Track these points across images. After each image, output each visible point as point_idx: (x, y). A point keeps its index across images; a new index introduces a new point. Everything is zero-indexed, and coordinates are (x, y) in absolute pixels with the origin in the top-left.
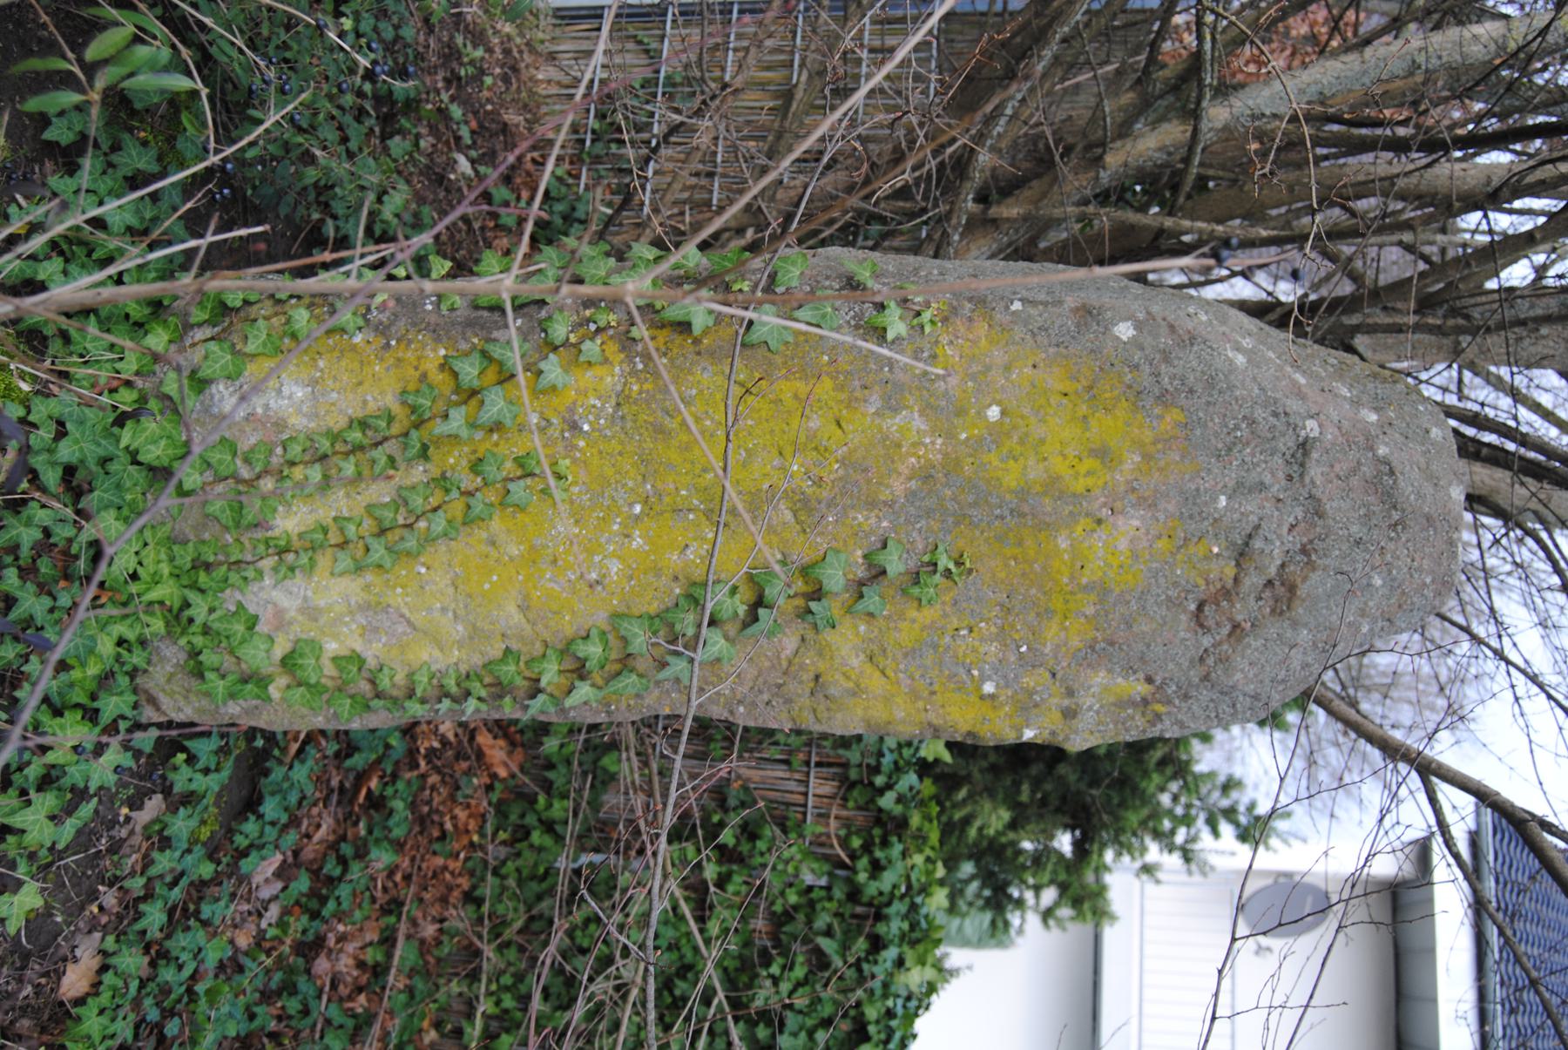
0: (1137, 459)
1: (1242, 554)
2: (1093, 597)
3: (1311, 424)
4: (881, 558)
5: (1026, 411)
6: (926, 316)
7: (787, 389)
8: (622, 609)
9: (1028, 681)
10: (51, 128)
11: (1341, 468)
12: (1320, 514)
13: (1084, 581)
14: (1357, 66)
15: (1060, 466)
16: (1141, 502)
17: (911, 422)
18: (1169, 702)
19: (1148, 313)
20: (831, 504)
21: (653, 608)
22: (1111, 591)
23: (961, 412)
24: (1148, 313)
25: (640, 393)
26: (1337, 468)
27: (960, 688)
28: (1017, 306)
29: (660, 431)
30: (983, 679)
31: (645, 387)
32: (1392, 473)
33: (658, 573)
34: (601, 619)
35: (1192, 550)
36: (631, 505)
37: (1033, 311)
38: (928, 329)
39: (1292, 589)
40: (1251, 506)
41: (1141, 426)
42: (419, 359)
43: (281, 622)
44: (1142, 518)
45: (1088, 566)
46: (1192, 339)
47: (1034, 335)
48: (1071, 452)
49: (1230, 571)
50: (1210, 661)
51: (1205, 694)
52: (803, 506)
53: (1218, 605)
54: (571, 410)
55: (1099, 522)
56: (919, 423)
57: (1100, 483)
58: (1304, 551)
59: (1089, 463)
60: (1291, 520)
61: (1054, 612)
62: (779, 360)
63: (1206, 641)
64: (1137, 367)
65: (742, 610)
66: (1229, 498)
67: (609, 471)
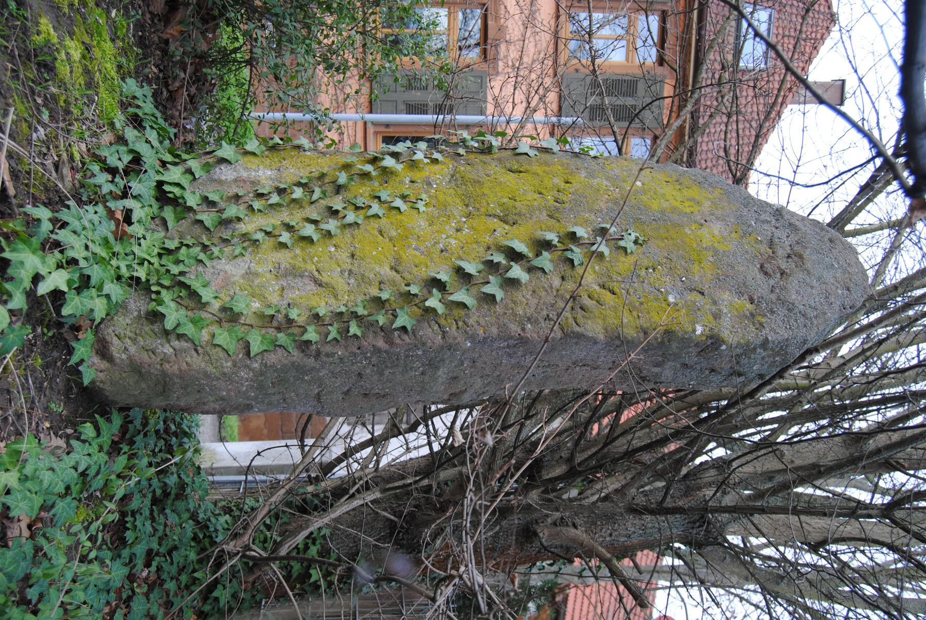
18: (764, 316)
30: (668, 293)
55: (702, 225)
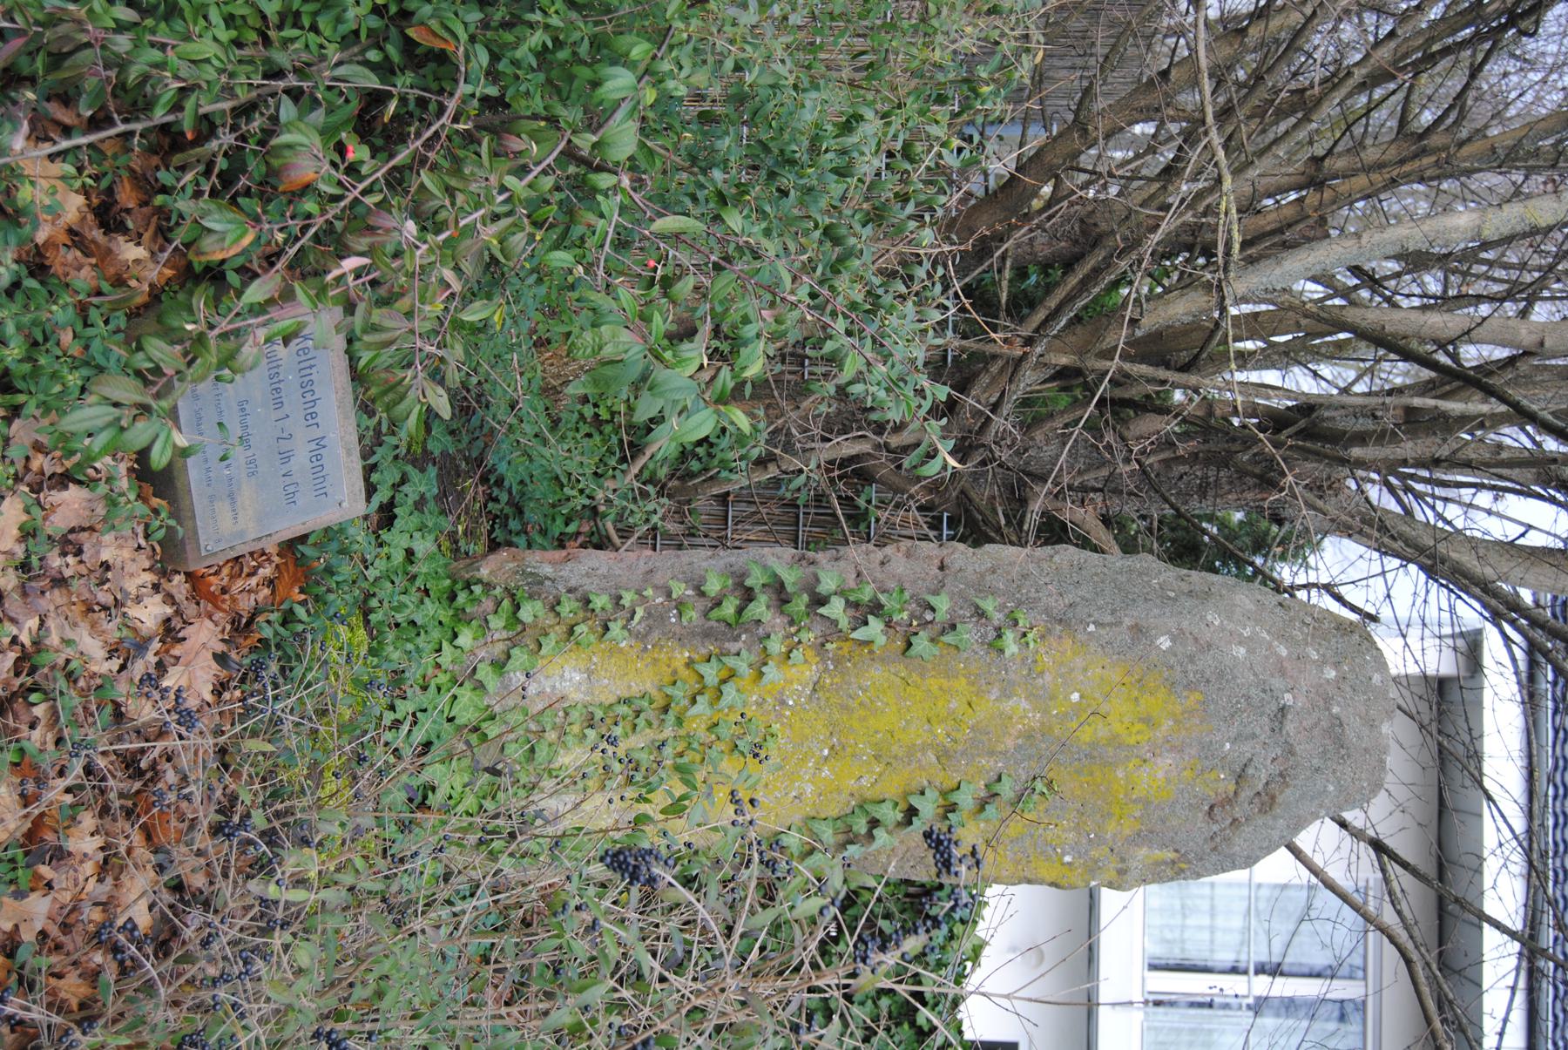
1: (1240, 777)
2: (1140, 806)
3: (1288, 696)
4: (997, 788)
5: (1097, 695)
6: (1030, 636)
7: (933, 683)
8: (813, 814)
9: (1094, 853)
12: (1292, 752)
14: (1355, 250)
15: (1118, 728)
16: (1173, 749)
17: (1019, 704)
18: (1190, 862)
20: (963, 753)
21: (835, 813)
23: (1053, 698)
28: (1092, 628)
29: (845, 708)
30: (1064, 854)
32: (1341, 725)
33: (839, 791)
34: (796, 819)
37: (1103, 632)
38: (1032, 645)
39: (1273, 798)
40: (1247, 749)
46: (1209, 646)
48: (1126, 720)
49: (1232, 788)
50: (1218, 839)
51: (1214, 857)
52: (944, 755)
54: (781, 693)
56: (1024, 704)
58: (1281, 775)
59: (1139, 726)
63: (1215, 828)
64: (1172, 667)
65: (900, 816)
67: (807, 731)
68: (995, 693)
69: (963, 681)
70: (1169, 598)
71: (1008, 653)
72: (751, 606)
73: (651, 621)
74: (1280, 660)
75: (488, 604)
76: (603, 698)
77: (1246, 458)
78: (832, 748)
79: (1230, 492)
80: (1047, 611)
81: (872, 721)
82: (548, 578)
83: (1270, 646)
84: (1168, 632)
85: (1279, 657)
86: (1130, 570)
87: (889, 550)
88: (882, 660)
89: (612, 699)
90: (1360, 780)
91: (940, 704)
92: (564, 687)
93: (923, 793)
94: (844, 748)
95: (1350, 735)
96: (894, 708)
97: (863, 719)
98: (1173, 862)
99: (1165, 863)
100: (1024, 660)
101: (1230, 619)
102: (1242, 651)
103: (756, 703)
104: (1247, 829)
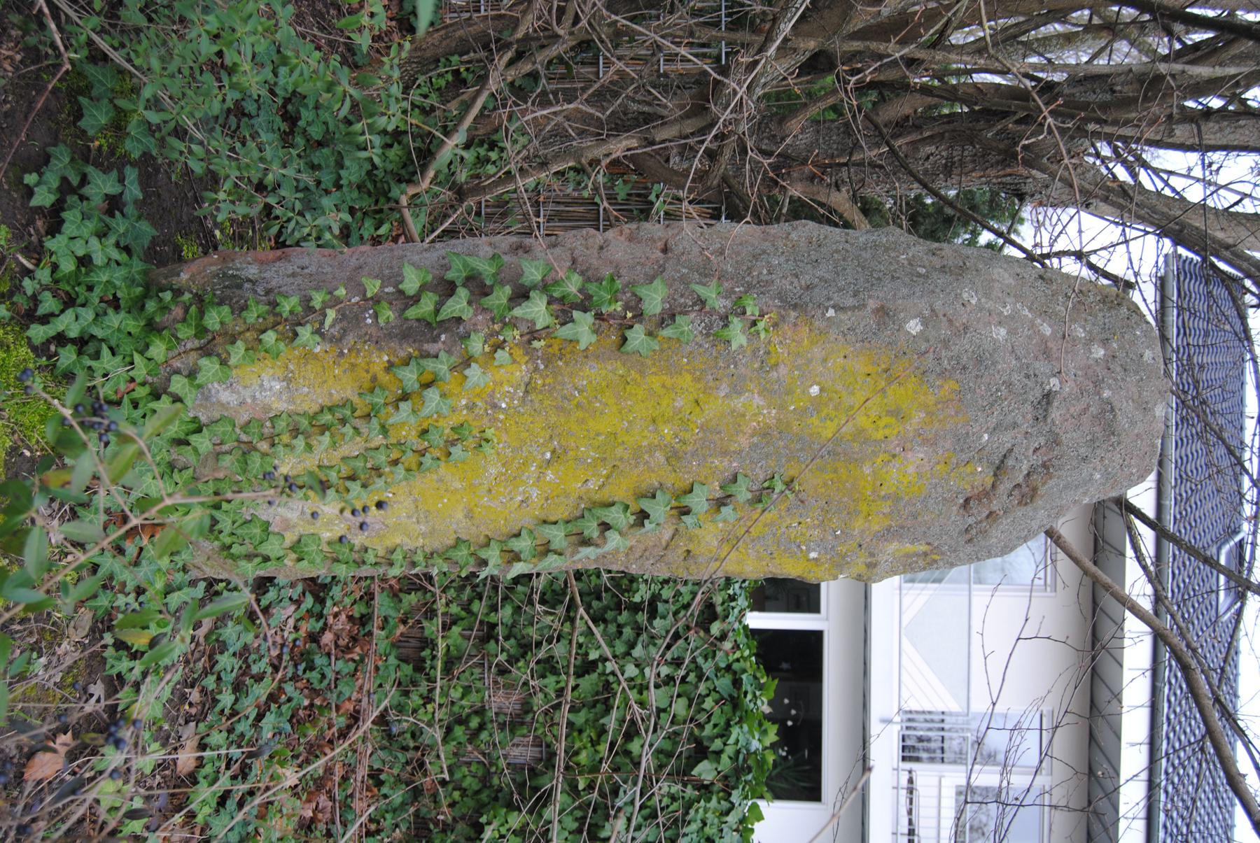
0: (922, 415)
1: (999, 469)
2: (889, 503)
4: (733, 489)
5: (839, 388)
6: (761, 325)
7: (655, 382)
9: (842, 549)
10: (35, 196)
11: (1076, 409)
12: (1057, 442)
13: (883, 493)
16: (925, 442)
19: (933, 310)
21: (566, 515)
22: (902, 499)
23: (789, 392)
24: (933, 310)
25: (544, 385)
26: (1072, 410)
27: (793, 555)
28: (831, 313)
29: (560, 409)
30: (809, 550)
31: (547, 381)
32: (1112, 410)
35: (962, 469)
36: (543, 454)
37: (843, 317)
38: (763, 335)
39: (1035, 490)
41: (925, 394)
42: (368, 364)
43: (287, 525)
44: (926, 453)
45: (885, 485)
47: (845, 335)
49: (989, 481)
50: (974, 532)
53: (980, 501)
54: (492, 395)
56: (758, 401)
57: (895, 432)
58: (1044, 465)
59: (886, 420)
60: (1036, 445)
61: (860, 512)
62: (649, 362)
63: (971, 520)
65: (632, 519)
66: (991, 434)
68: (724, 389)
69: (688, 378)
70: (919, 275)
71: (734, 346)
72: (450, 302)
73: (345, 323)
74: (1044, 341)
75: (178, 312)
76: (305, 407)
77: (990, 135)
78: (553, 452)
79: (973, 170)
80: (781, 296)
81: (591, 423)
82: (249, 280)
83: (1032, 325)
84: (919, 314)
85: (1042, 337)
86: (876, 246)
87: (610, 234)
88: (598, 357)
89: (316, 408)
90: (1129, 466)
91: (664, 403)
92: (267, 398)
93: (654, 496)
94: (566, 452)
95: (1122, 421)
96: (614, 409)
97: (582, 422)
98: (925, 554)
99: (916, 555)
100: (755, 352)
101: (987, 296)
102: (1003, 332)
103: (467, 407)
104: (1005, 522)
